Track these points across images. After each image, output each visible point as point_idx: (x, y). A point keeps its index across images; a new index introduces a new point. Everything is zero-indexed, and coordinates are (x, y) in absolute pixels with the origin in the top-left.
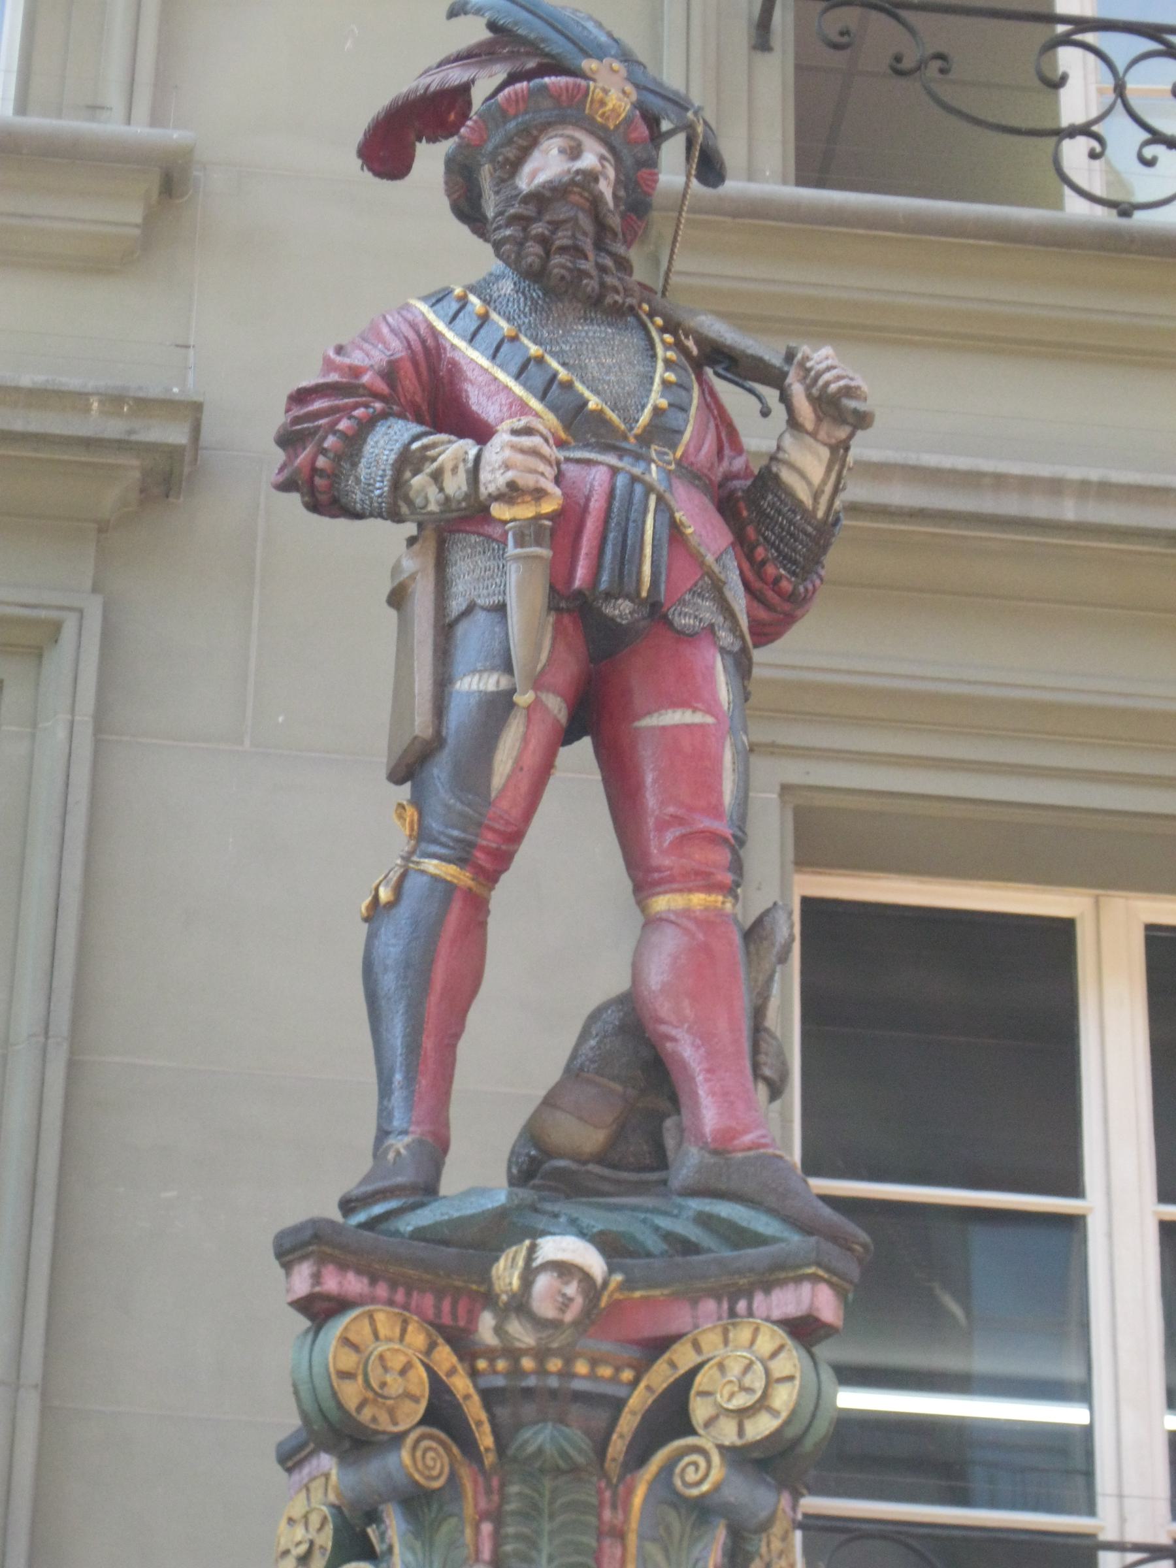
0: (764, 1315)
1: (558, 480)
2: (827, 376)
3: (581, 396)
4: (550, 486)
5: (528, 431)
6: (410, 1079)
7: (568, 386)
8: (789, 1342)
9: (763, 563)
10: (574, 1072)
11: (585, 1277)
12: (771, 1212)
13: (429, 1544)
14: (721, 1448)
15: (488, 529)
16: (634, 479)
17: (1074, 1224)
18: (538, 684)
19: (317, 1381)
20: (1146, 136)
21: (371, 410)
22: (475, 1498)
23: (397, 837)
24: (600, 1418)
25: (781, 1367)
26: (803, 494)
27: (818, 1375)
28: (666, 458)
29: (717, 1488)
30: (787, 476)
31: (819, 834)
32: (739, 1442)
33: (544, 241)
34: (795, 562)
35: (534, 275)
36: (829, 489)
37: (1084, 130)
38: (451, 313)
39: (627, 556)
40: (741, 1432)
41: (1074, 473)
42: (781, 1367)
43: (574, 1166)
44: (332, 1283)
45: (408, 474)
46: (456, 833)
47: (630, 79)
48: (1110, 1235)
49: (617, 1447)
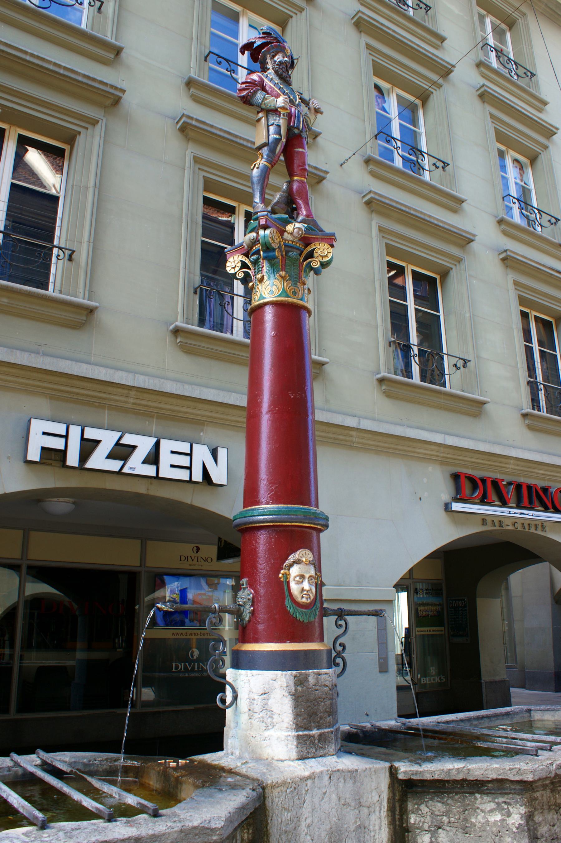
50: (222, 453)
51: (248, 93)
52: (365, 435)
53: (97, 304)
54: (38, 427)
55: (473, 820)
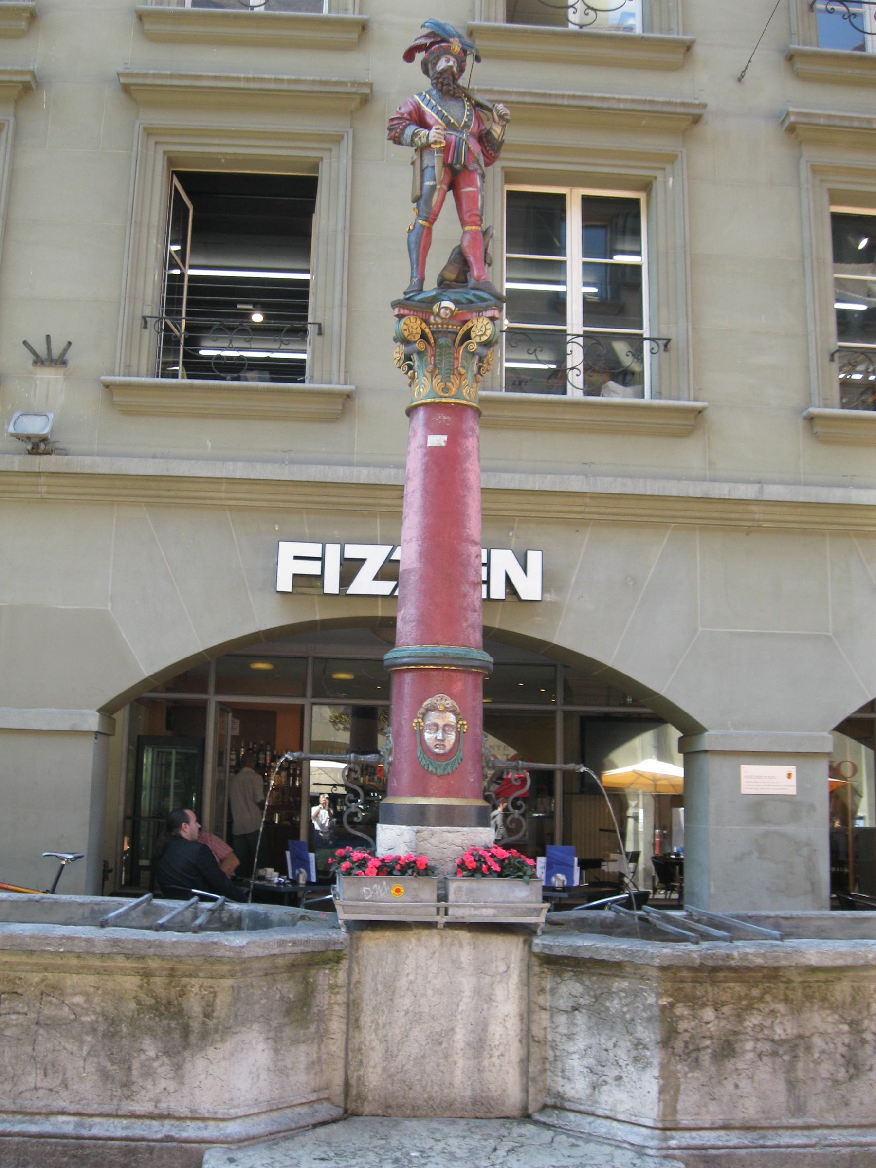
1: (445, 139)
5: (438, 129)
6: (417, 266)
10: (450, 262)
11: (451, 309)
12: (488, 293)
17: (565, 262)
18: (441, 183)
23: (414, 215)
24: (453, 336)
25: (488, 326)
26: (496, 136)
30: (493, 132)
31: (509, 177)
33: (442, 83)
35: (440, 90)
41: (567, 93)
42: (488, 326)
44: (402, 312)
47: (460, 42)
49: (457, 342)
50: (535, 559)
52: (776, 509)
53: (353, 387)
54: (287, 550)
55: (608, 1004)
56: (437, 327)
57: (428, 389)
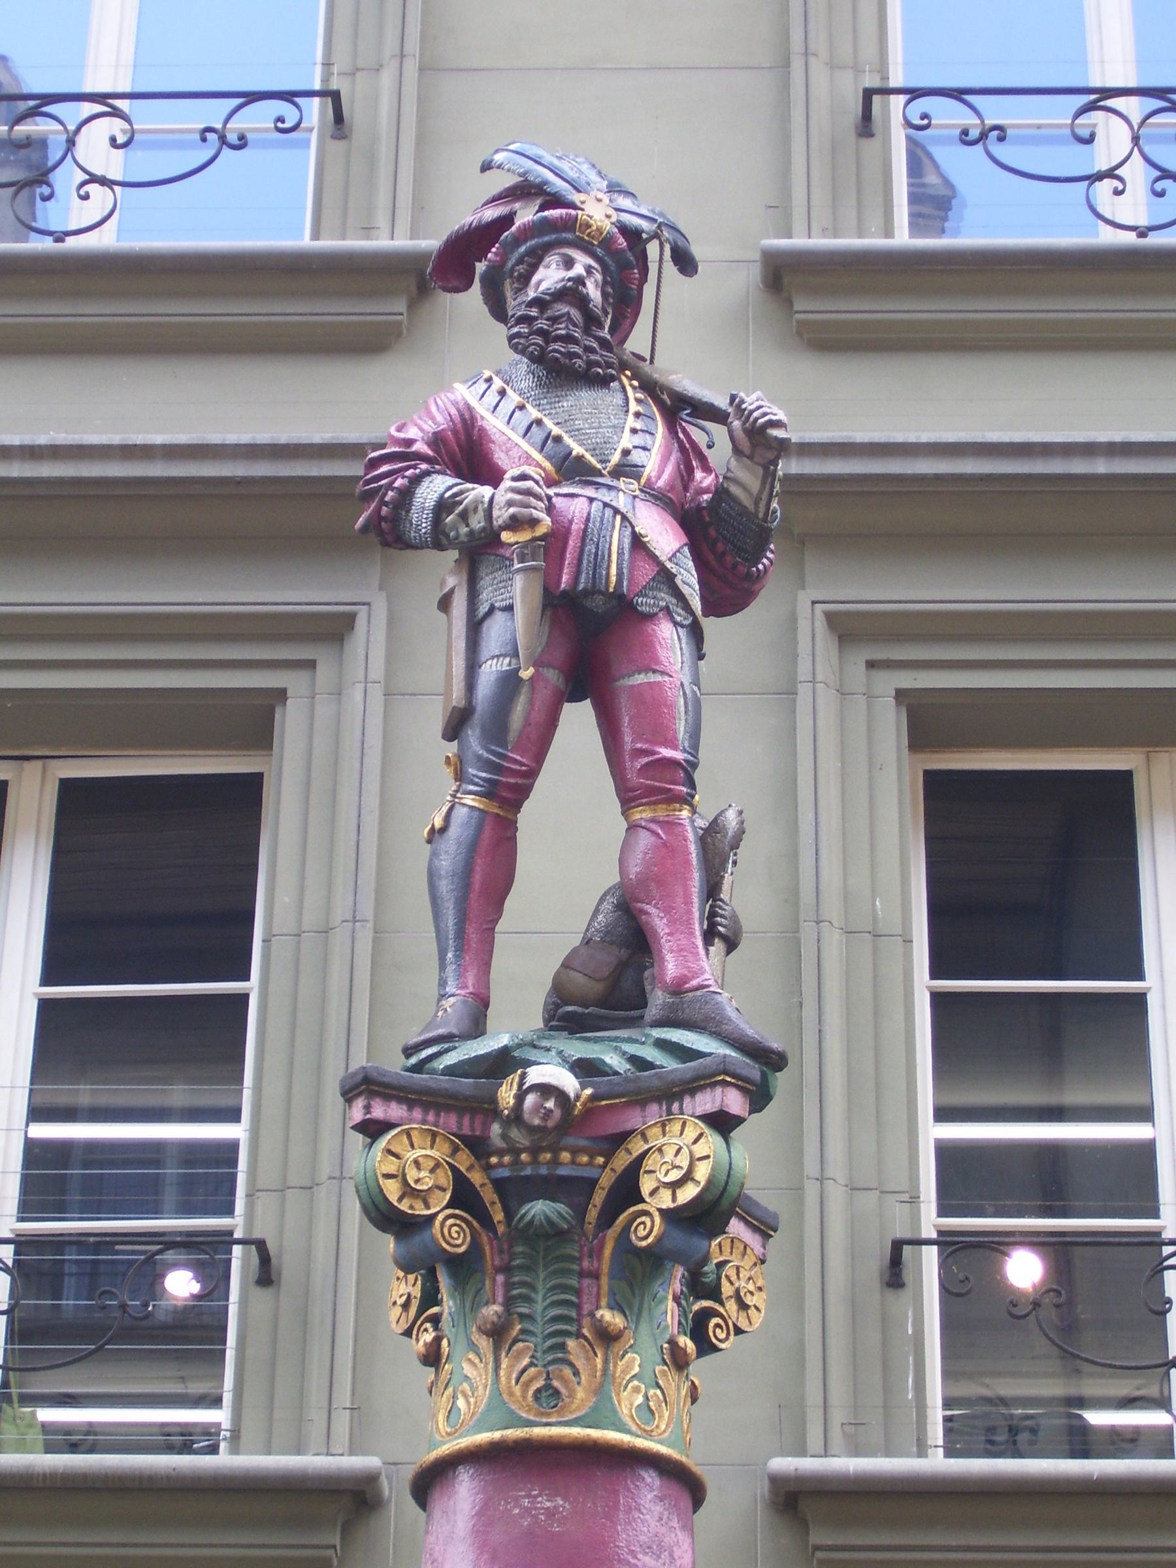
0: (690, 1112)
2: (756, 414)
3: (568, 446)
4: (542, 515)
5: (524, 477)
7: (558, 439)
8: (707, 1131)
9: (723, 554)
13: (463, 1294)
14: (660, 1210)
15: (502, 551)
16: (606, 505)
17: (1139, 1001)
19: (369, 1182)
20: (1158, 173)
21: (418, 471)
22: (492, 1259)
25: (700, 1149)
27: (729, 1151)
28: (631, 487)
29: (659, 1239)
32: (672, 1206)
34: (746, 552)
36: (765, 496)
37: (1110, 174)
38: (481, 392)
39: (600, 561)
40: (674, 1199)
42: (700, 1149)
43: (580, 1010)
44: (379, 1111)
45: (444, 515)
46: (484, 775)
48: (1164, 1007)
49: (592, 1214)
51: (378, 510)
56: (516, 1162)
57: (484, 1395)
